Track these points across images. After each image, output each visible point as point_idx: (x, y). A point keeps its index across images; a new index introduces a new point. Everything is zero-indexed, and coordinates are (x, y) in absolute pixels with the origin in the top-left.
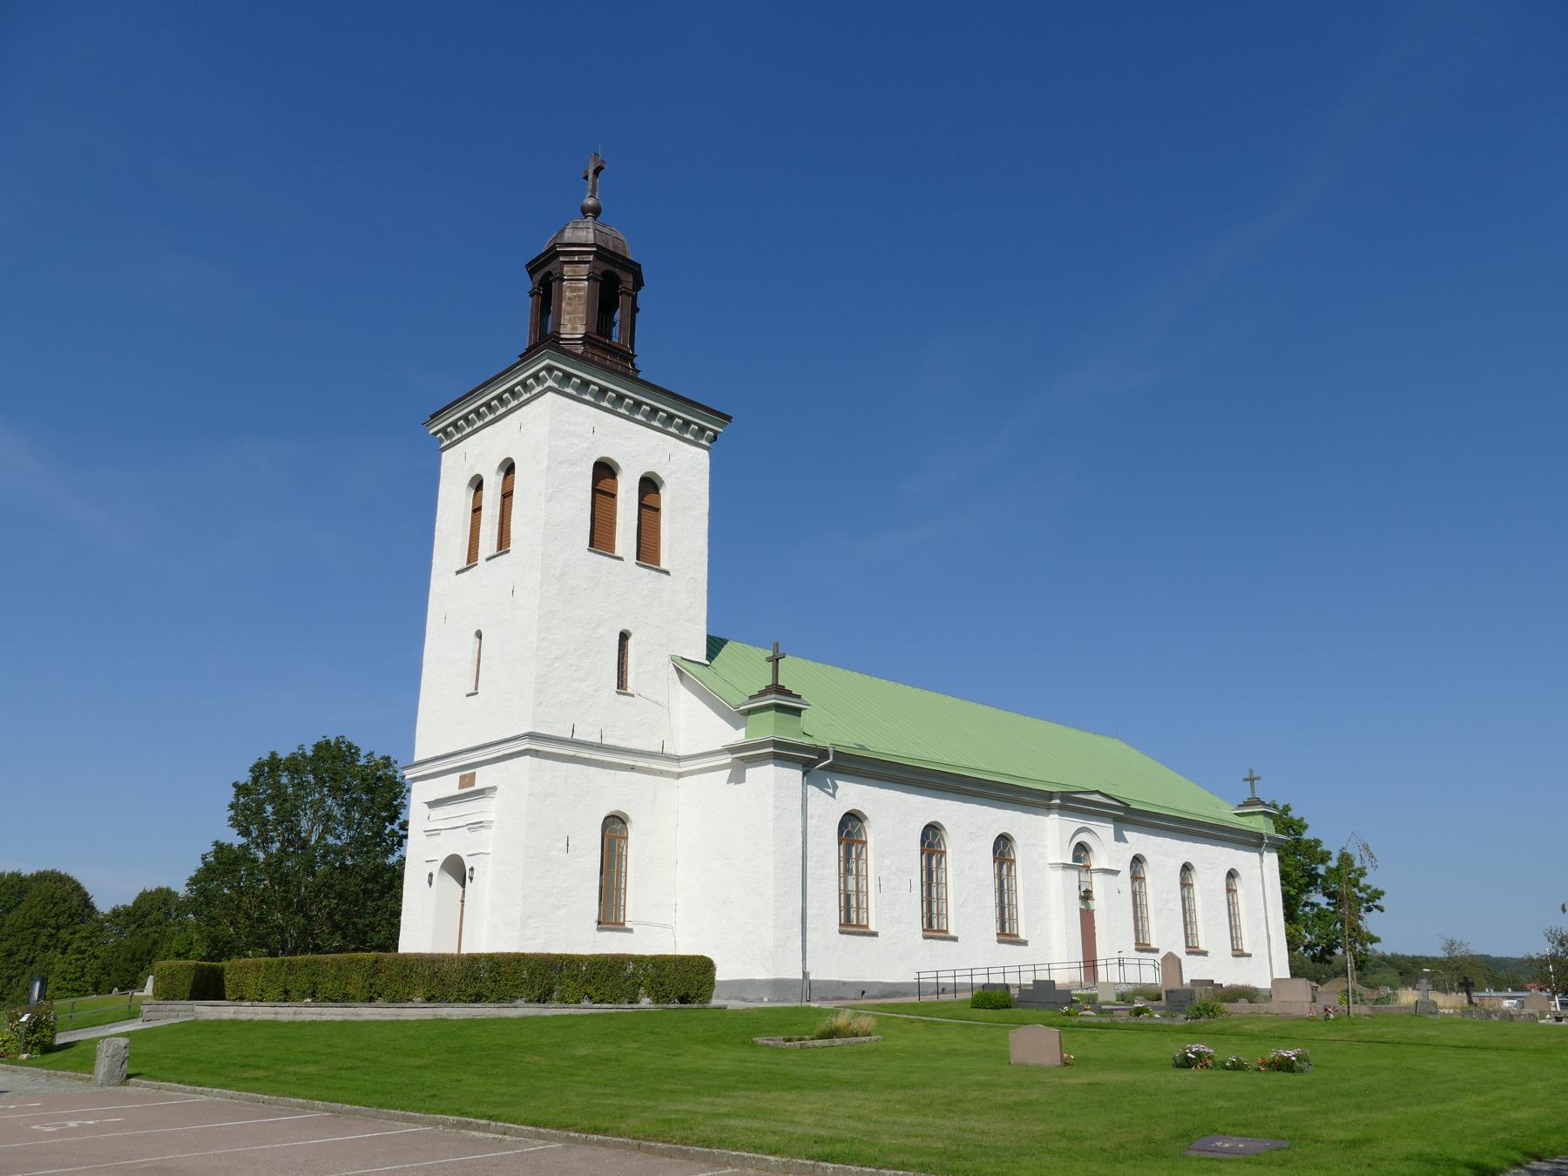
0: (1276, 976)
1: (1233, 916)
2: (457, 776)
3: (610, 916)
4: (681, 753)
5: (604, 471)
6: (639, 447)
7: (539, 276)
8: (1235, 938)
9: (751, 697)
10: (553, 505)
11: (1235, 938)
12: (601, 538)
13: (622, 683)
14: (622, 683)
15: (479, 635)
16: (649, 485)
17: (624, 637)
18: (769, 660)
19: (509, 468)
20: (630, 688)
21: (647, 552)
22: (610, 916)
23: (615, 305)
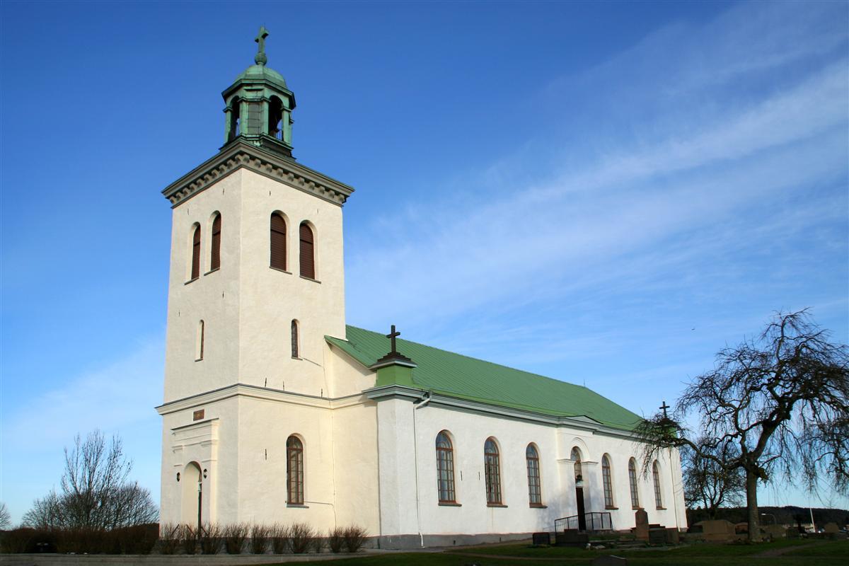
0: (375, 407)
1: (202, 351)
2: (191, 412)
3: (296, 497)
4: (332, 398)
5: (278, 219)
6: (300, 205)
7: (230, 100)
8: (658, 500)
9: (380, 361)
10: (249, 240)
11: (658, 500)
12: (278, 261)
13: (295, 354)
14: (295, 354)
15: (202, 321)
16: (305, 227)
17: (294, 323)
18: (399, 334)
19: (218, 217)
20: (301, 353)
21: (308, 270)
22: (296, 497)
23: (280, 117)
